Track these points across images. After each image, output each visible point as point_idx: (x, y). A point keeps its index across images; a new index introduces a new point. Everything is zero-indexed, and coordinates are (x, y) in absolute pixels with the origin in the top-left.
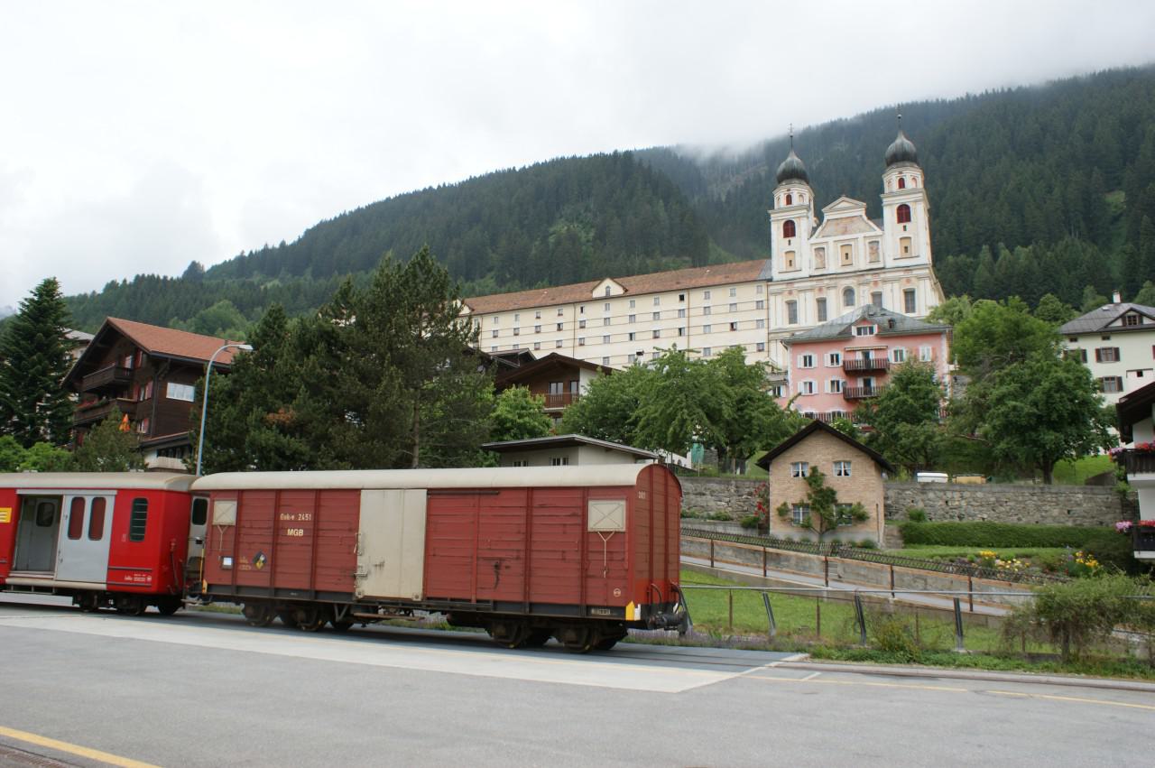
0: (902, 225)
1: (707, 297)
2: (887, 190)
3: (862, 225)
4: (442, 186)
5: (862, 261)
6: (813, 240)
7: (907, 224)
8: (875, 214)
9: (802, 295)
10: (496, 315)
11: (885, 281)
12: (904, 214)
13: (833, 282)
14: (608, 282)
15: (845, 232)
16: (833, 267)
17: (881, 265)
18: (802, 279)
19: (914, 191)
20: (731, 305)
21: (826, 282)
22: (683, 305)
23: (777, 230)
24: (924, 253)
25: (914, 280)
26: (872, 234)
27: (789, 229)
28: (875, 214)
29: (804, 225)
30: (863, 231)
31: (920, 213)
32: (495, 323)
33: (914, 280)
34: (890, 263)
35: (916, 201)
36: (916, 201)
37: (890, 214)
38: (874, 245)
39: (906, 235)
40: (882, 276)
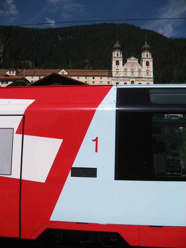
0: (147, 67)
1: (94, 78)
2: (113, 56)
3: (137, 65)
4: (182, 38)
5: (136, 75)
6: (124, 67)
7: (118, 66)
8: (140, 62)
9: (121, 81)
10: (101, 76)
11: (142, 81)
12: (148, 64)
13: (129, 79)
14: (63, 70)
15: (133, 66)
16: (129, 75)
17: (141, 76)
18: (121, 77)
19: (120, 58)
20: (101, 82)
21: (127, 79)
22: (94, 80)
23: (114, 63)
24: (151, 75)
25: (119, 80)
26: (139, 67)
27: (117, 63)
28: (140, 62)
29: (121, 63)
30: (137, 67)
31: (151, 64)
32: (85, 79)
33: (119, 80)
34: (144, 76)
35: (151, 61)
36: (151, 61)
37: (144, 63)
38: (140, 71)
39: (148, 69)
40: (142, 79)
